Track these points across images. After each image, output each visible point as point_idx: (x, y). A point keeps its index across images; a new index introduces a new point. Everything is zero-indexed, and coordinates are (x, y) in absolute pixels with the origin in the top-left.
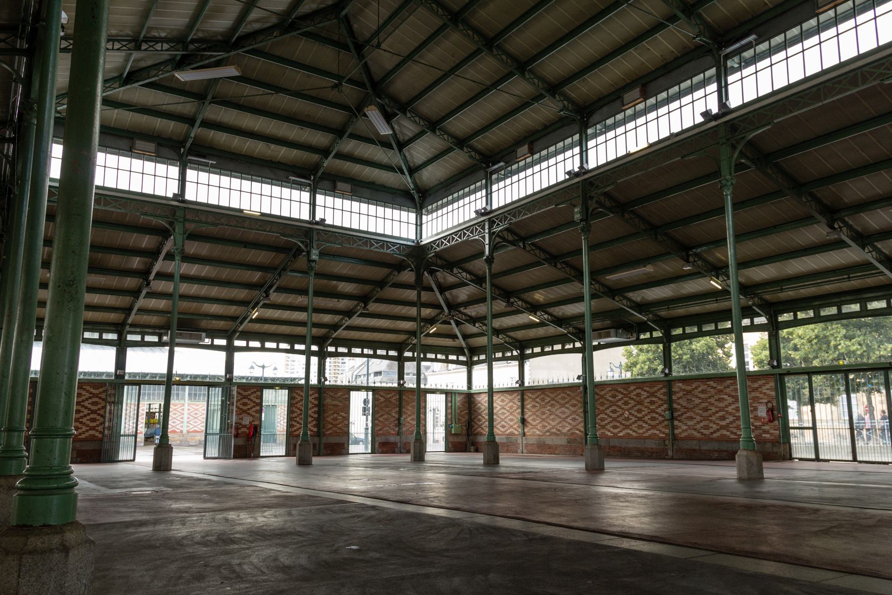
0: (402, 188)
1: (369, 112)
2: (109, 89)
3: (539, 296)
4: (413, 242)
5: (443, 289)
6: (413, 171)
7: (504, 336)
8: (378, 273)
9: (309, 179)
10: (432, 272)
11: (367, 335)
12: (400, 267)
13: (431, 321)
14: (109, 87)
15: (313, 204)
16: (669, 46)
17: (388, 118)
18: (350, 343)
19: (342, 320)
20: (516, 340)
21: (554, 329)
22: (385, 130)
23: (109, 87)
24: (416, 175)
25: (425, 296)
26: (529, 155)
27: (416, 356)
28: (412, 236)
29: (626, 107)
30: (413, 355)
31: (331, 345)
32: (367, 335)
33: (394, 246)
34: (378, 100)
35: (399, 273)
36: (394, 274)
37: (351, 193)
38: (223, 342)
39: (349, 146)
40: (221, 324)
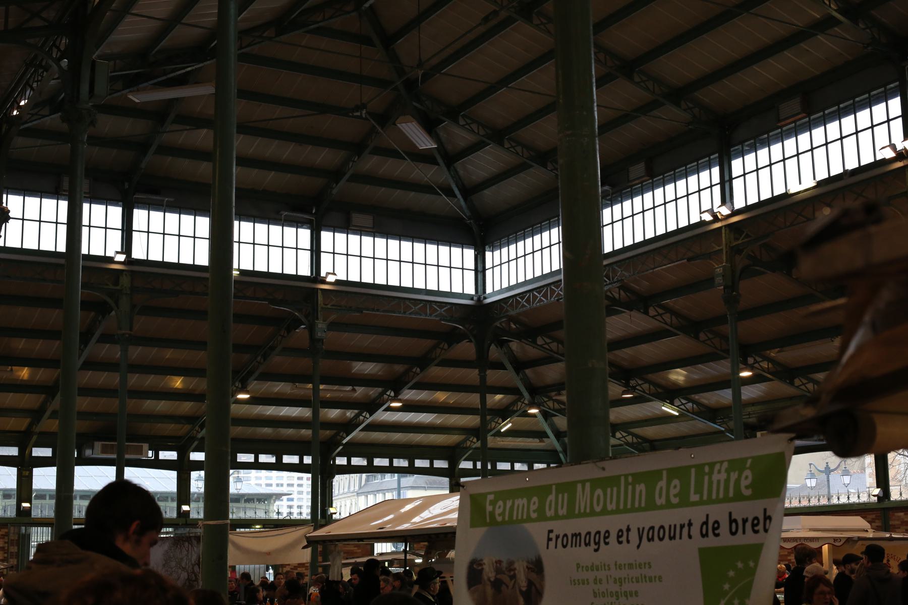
0: (549, 448)
1: (404, 124)
2: (35, 117)
3: (678, 376)
4: (472, 299)
5: (519, 366)
6: (469, 191)
7: (625, 434)
8: (419, 346)
9: (310, 213)
10: (501, 344)
11: (397, 437)
12: (452, 337)
13: (504, 413)
14: (36, 114)
15: (316, 251)
16: (834, 47)
17: (430, 126)
18: (369, 450)
19: (357, 416)
20: (645, 440)
21: (705, 424)
22: (425, 143)
23: (36, 114)
24: (458, 165)
25: (493, 376)
26: (647, 178)
27: (47, 452)
28: (470, 289)
29: (783, 123)
30: (475, 465)
31: (340, 455)
32: (397, 437)
33: (441, 307)
34: (415, 104)
35: (449, 346)
36: (441, 346)
37: (373, 228)
38: (172, 455)
39: (370, 163)
40: (170, 429)
